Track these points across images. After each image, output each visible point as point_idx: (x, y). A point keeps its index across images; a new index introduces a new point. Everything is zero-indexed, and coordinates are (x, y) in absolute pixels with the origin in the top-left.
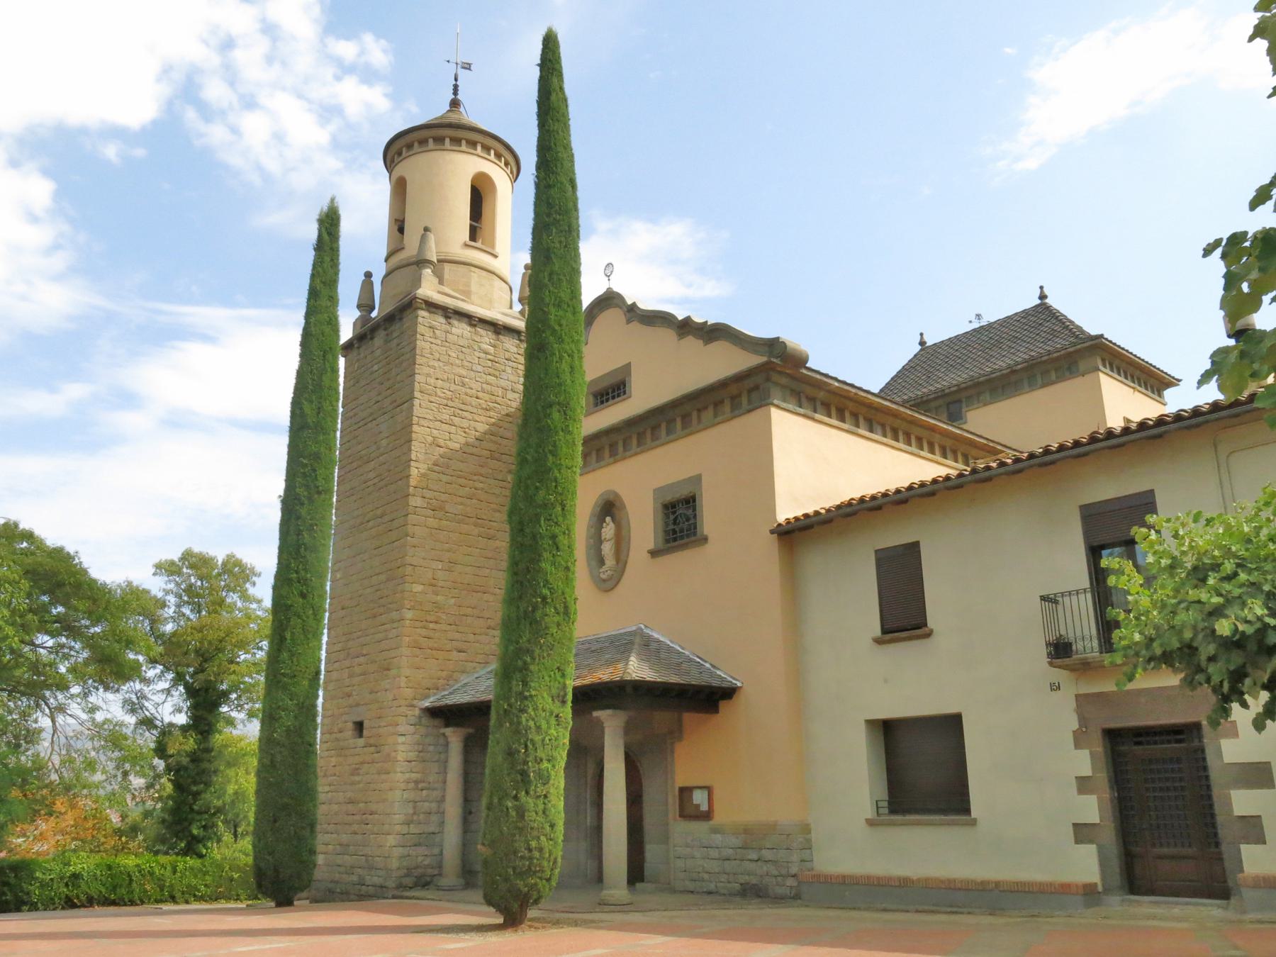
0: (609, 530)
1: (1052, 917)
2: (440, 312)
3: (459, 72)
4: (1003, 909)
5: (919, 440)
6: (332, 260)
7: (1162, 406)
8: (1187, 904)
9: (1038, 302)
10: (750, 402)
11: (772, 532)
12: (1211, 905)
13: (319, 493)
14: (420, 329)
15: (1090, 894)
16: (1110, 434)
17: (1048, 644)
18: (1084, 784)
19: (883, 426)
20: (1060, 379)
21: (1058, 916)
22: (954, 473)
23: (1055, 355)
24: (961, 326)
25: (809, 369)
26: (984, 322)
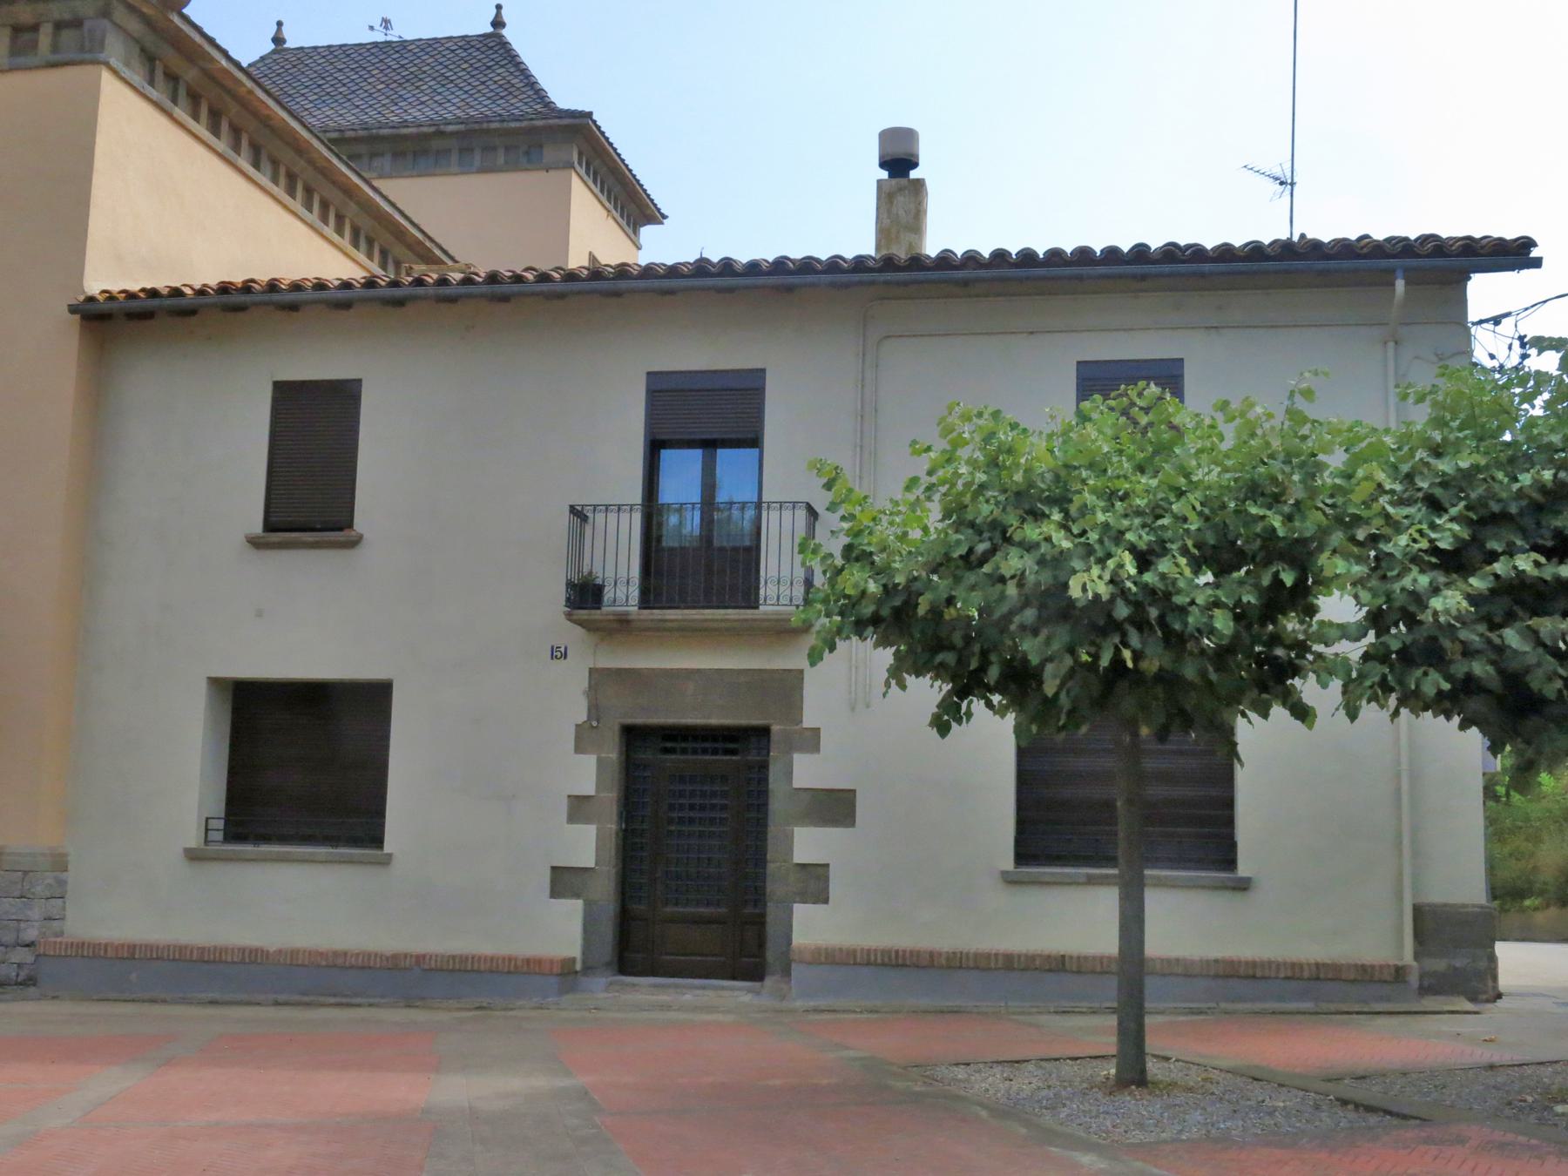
1: (512, 1009)
4: (423, 999)
5: (325, 206)
7: (634, 248)
8: (704, 988)
9: (490, 29)
10: (55, 48)
11: (73, 309)
12: (740, 989)
15: (567, 975)
16: (571, 276)
17: (570, 585)
18: (579, 808)
19: (275, 163)
20: (511, 166)
21: (520, 1008)
22: (355, 273)
23: (513, 125)
24: (355, 31)
25: (186, 19)
26: (393, 37)
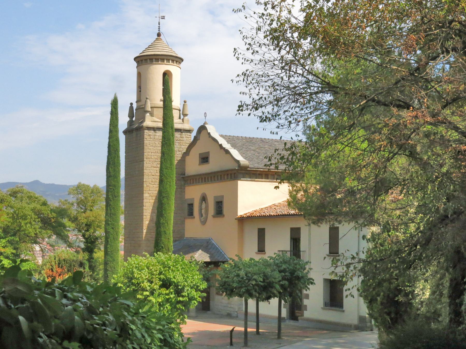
0: (204, 205)
2: (152, 129)
3: (160, 21)
6: (116, 117)
13: (116, 197)
14: (145, 136)
